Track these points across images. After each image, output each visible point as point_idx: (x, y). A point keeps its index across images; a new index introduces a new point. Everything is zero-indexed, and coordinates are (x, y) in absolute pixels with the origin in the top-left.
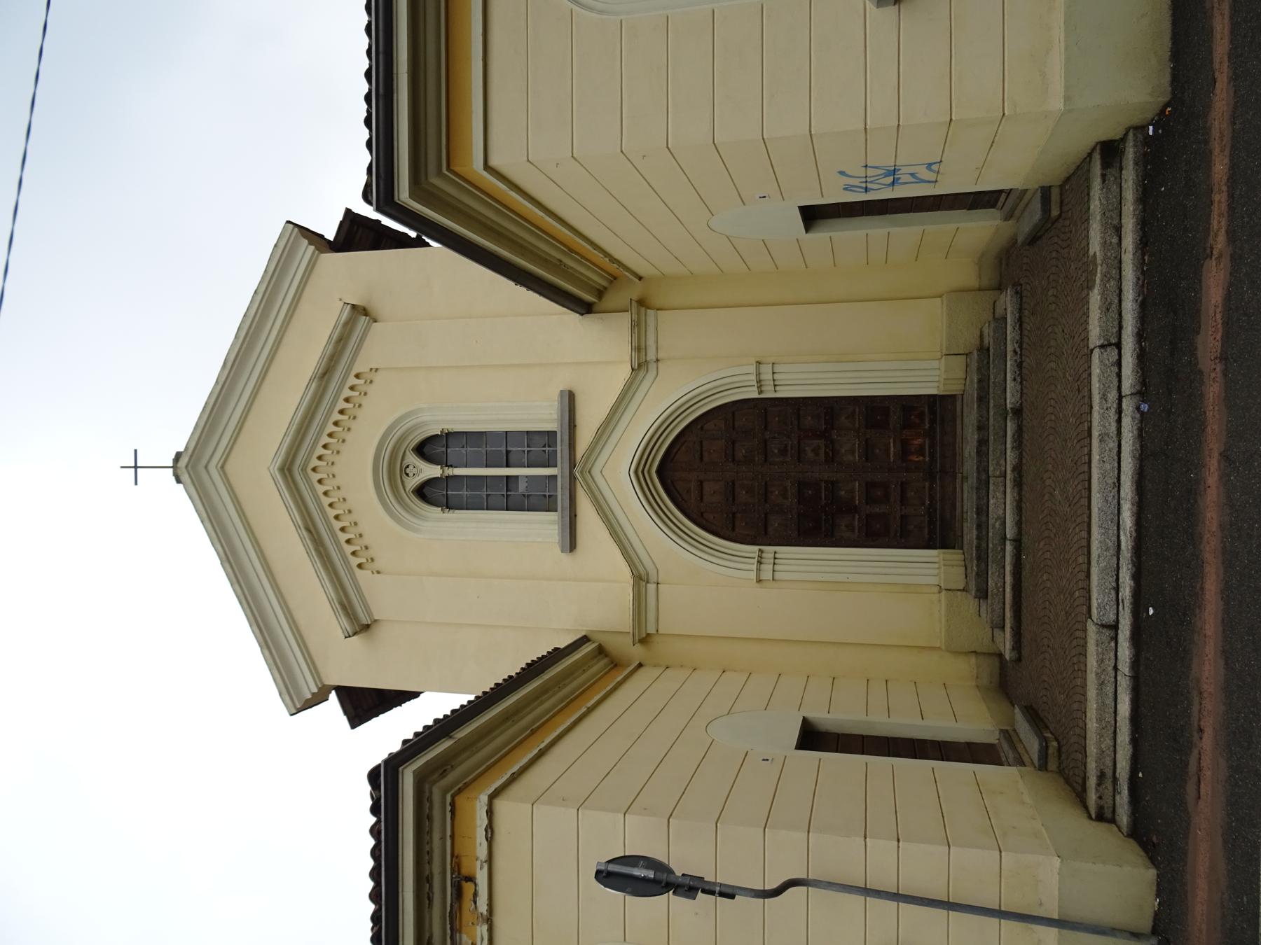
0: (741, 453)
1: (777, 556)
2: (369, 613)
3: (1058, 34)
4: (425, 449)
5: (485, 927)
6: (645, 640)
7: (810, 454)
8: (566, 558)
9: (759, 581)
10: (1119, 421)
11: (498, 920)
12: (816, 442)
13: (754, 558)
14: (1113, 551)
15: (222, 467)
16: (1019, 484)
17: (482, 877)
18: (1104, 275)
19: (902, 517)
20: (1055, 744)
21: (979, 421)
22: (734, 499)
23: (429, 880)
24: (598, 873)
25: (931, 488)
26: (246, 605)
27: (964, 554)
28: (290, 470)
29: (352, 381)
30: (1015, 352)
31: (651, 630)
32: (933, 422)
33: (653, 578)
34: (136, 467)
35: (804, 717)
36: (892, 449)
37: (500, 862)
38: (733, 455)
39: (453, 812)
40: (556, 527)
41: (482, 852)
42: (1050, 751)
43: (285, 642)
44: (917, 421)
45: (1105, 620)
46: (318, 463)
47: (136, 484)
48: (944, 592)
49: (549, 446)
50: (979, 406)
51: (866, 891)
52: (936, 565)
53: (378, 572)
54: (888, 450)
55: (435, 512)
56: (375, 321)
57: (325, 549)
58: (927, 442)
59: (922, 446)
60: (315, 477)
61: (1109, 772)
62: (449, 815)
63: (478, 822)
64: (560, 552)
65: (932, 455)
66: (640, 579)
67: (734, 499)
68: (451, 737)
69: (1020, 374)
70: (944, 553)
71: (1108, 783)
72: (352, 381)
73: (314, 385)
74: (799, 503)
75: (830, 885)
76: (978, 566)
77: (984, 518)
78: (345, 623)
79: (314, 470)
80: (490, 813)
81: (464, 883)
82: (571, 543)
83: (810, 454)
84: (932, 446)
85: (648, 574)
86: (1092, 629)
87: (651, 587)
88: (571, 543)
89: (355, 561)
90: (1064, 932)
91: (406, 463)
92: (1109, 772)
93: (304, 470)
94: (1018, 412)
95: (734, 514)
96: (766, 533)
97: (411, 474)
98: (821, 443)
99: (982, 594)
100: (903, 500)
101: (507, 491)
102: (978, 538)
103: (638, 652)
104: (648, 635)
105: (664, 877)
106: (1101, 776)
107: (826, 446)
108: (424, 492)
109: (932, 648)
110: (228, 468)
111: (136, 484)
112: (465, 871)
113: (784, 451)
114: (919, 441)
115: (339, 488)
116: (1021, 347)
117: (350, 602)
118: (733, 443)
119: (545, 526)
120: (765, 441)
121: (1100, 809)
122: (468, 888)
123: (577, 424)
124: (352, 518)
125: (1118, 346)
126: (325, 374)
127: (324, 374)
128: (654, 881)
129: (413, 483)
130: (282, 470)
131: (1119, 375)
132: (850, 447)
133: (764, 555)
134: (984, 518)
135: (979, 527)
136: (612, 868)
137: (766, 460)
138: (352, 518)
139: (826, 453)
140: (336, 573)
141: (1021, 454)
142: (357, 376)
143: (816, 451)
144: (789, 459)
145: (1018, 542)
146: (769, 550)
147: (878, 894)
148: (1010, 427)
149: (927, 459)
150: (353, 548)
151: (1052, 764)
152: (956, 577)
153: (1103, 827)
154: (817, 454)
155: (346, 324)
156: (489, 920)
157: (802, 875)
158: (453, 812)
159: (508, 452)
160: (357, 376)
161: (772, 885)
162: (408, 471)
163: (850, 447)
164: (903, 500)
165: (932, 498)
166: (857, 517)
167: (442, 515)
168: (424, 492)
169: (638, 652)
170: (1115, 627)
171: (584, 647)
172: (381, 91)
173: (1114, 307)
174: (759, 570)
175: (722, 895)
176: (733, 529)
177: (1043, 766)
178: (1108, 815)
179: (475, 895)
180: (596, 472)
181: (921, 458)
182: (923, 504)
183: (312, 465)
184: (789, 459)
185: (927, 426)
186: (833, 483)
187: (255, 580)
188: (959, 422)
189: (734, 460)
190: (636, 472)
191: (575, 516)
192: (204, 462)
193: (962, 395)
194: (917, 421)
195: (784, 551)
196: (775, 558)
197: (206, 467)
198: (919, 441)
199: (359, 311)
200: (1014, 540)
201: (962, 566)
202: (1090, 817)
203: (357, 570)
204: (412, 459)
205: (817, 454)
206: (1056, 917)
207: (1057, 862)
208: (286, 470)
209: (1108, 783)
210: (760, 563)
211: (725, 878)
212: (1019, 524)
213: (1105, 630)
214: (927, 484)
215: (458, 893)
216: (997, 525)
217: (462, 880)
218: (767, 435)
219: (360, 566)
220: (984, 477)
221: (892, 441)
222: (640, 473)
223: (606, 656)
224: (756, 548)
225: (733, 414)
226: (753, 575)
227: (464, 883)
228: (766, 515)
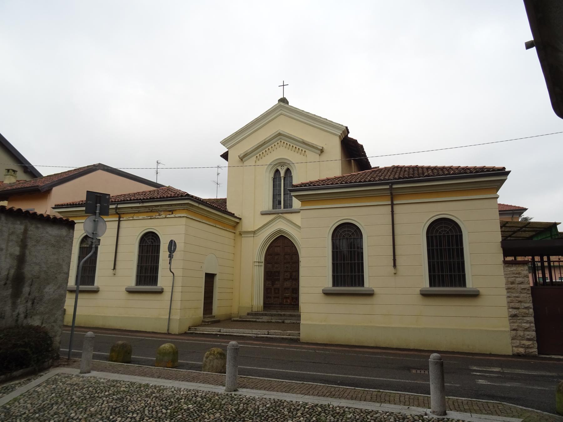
0: (287, 257)
1: (261, 266)
2: (245, 161)
3: (314, 323)
4: (288, 171)
5: (164, 217)
6: (240, 234)
7: (286, 274)
8: (259, 213)
9: (254, 262)
10: (255, 334)
11: (166, 219)
12: (289, 276)
13: (260, 261)
14: (232, 332)
15: (282, 114)
16: (268, 322)
17: (172, 216)
18: (281, 332)
19: (271, 297)
20: (207, 324)
21: (286, 314)
22: (276, 255)
23: (171, 206)
24: (172, 240)
25: (278, 304)
26: (246, 126)
27: (259, 311)
28: (280, 135)
29: (304, 150)
30: (297, 322)
31: (243, 235)
32: (293, 305)
33: (255, 235)
34: (284, 85)
35: (216, 274)
36: (287, 295)
37: (175, 219)
38: (286, 255)
39: (183, 209)
40: (267, 210)
41: (177, 216)
42: (206, 323)
43: (239, 137)
44: (294, 301)
45: (221, 330)
46: (283, 142)
47: (279, 86)
48: (251, 306)
49: (289, 205)
50: (289, 315)
51: (173, 286)
52: (258, 305)
53: (255, 162)
54: (287, 293)
55: (272, 175)
56: (319, 155)
57: (260, 147)
58: (288, 303)
59: (288, 302)
60: (279, 142)
61: (196, 330)
62: (182, 208)
63: (182, 214)
64: (261, 211)
65: (285, 304)
66: (254, 232)
67: (276, 255)
68: (199, 205)
69: (292, 323)
70: (261, 307)
71: (195, 330)
72: (304, 150)
73: (301, 140)
74: (275, 272)
75: (173, 280)
76: (254, 313)
77: (264, 315)
78: (242, 155)
79: (281, 141)
80: (183, 217)
81: (171, 212)
82: (263, 214)
83: (286, 274)
84: (288, 304)
85: (256, 234)
86: (220, 328)
87: (252, 235)
88: (263, 214)
89: (258, 155)
90: (168, 319)
91: (284, 166)
92: (196, 330)
93: (281, 139)
94: (283, 322)
95: (271, 255)
96: (267, 263)
97: (282, 168)
98: (289, 277)
99: (248, 314)
100: (275, 297)
101: (278, 195)
102: (260, 314)
103: (237, 233)
104: (241, 235)
105: (172, 252)
106: (196, 329)
107: (288, 278)
108: (277, 171)
109: (239, 303)
110: (282, 116)
111: (279, 86)
112: (174, 212)
113: (287, 267)
114: (289, 301)
115: (271, 152)
116: (298, 323)
117: (248, 155)
118: (289, 255)
119: (268, 205)
120: (289, 263)
121: (191, 328)
122: (171, 213)
123: (292, 214)
124: (275, 149)
125: (268, 334)
126: (304, 143)
127: (304, 143)
128: (171, 250)
129: (279, 168)
130: (279, 133)
131: (263, 334)
132: (288, 284)
133: (261, 263)
134: (264, 315)
135: (262, 314)
136: (173, 243)
137: (285, 263)
138: (275, 149)
139: (286, 278)
140: (254, 151)
141: (274, 323)
142: (305, 151)
143: (287, 276)
144: (285, 269)
145: (256, 321)
146: (263, 264)
147: (173, 289)
148: (280, 321)
149: (285, 303)
150: (264, 152)
151: (203, 323)
152: (255, 309)
153: (188, 329)
154: (286, 276)
155: (317, 148)
156: (166, 218)
157: (175, 275)
158: (183, 209)
159: (288, 194)
160: (305, 151)
161: (172, 270)
162: (283, 167)
163: (288, 284)
164: (275, 297)
165: (275, 304)
166: (271, 286)
167: (271, 177)
168: (277, 171)
169: (237, 233)
170: (220, 332)
171: (238, 219)
172: (311, 188)
173: (275, 334)
174: (257, 262)
175: (170, 262)
176: (268, 255)
177: (203, 321)
178: (190, 330)
179: (170, 214)
180: (280, 219)
181: (285, 302)
182: (274, 302)
183: (282, 140)
184: (285, 269)
185: (292, 303)
186: (279, 280)
187: (252, 128)
188: (293, 311)
189: (285, 255)
190: (280, 230)
191: (270, 215)
192: (282, 109)
193: (298, 312)
194: (294, 301)
195: (262, 269)
196: (260, 266)
197: (281, 110)
198: (289, 301)
199: (322, 151)
200: (256, 321)
201: (258, 310)
202: (189, 327)
203: (256, 156)
204: (285, 168)
205: (286, 276)
206: (170, 318)
207: (179, 318)
208: (280, 134)
209: (195, 330)
210: (259, 262)
211: (173, 261)
212: (259, 322)
213: (219, 330)
214: (278, 303)
215: (170, 211)
216: (261, 318)
217: (172, 212)
218: (291, 263)
219: (257, 157)
220: (273, 315)
221: (289, 295)
222: (280, 231)
223: (237, 224)
224: (263, 261)
225: (296, 254)
226: (256, 261)
227: (171, 212)
228: (271, 263)
